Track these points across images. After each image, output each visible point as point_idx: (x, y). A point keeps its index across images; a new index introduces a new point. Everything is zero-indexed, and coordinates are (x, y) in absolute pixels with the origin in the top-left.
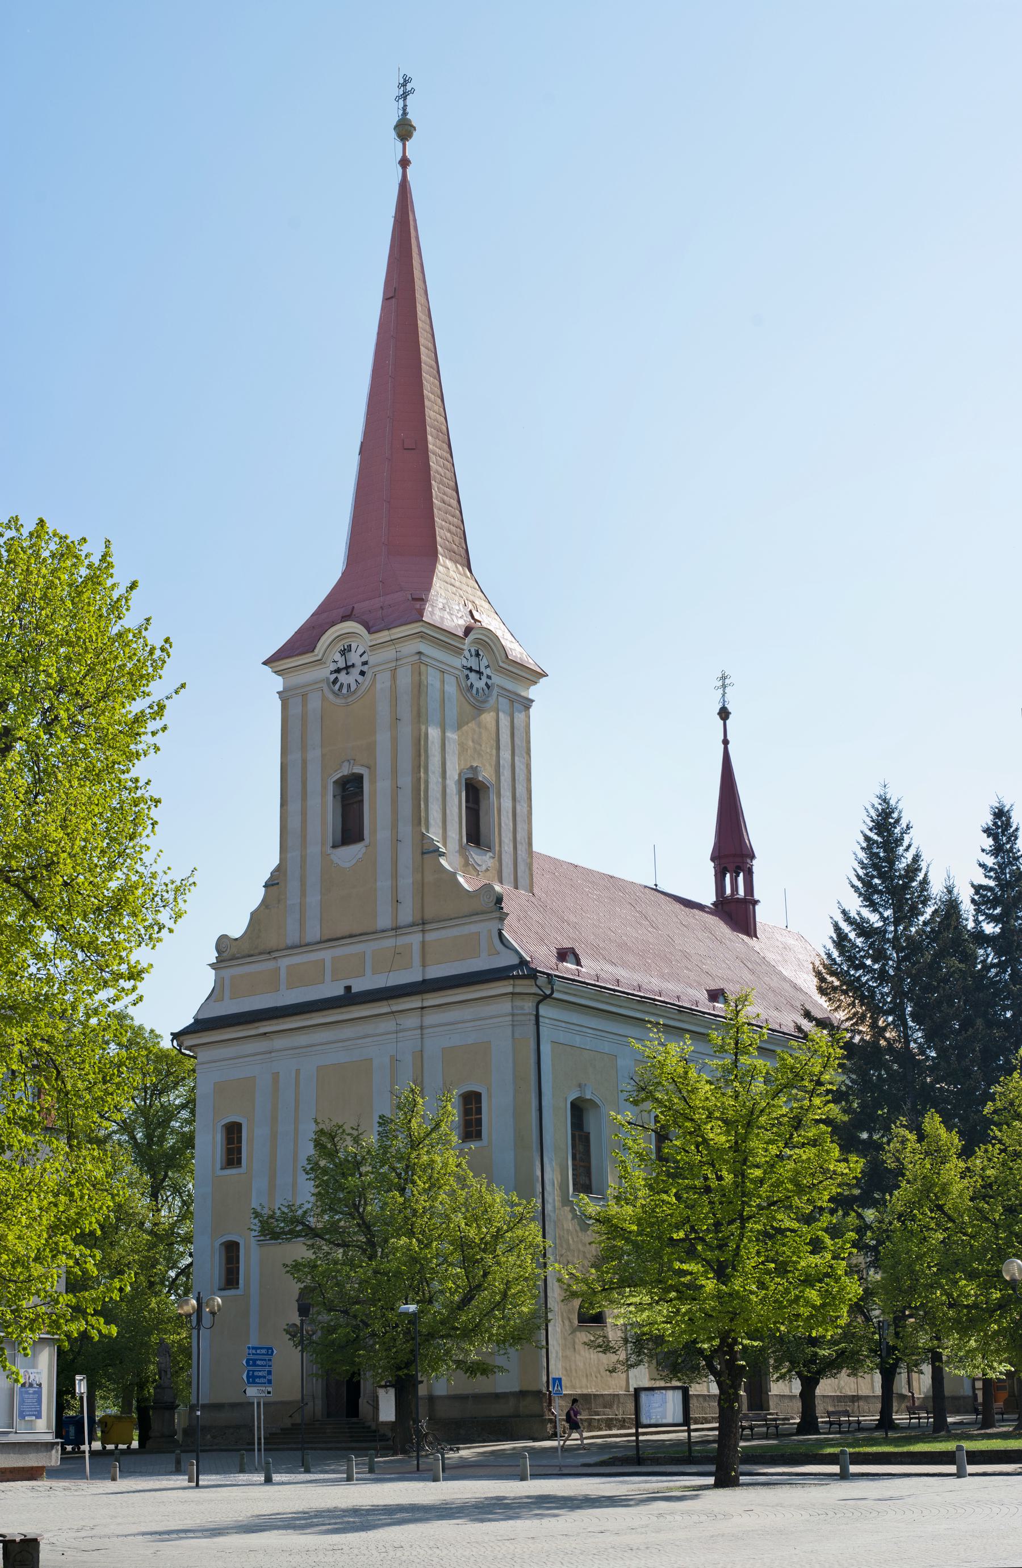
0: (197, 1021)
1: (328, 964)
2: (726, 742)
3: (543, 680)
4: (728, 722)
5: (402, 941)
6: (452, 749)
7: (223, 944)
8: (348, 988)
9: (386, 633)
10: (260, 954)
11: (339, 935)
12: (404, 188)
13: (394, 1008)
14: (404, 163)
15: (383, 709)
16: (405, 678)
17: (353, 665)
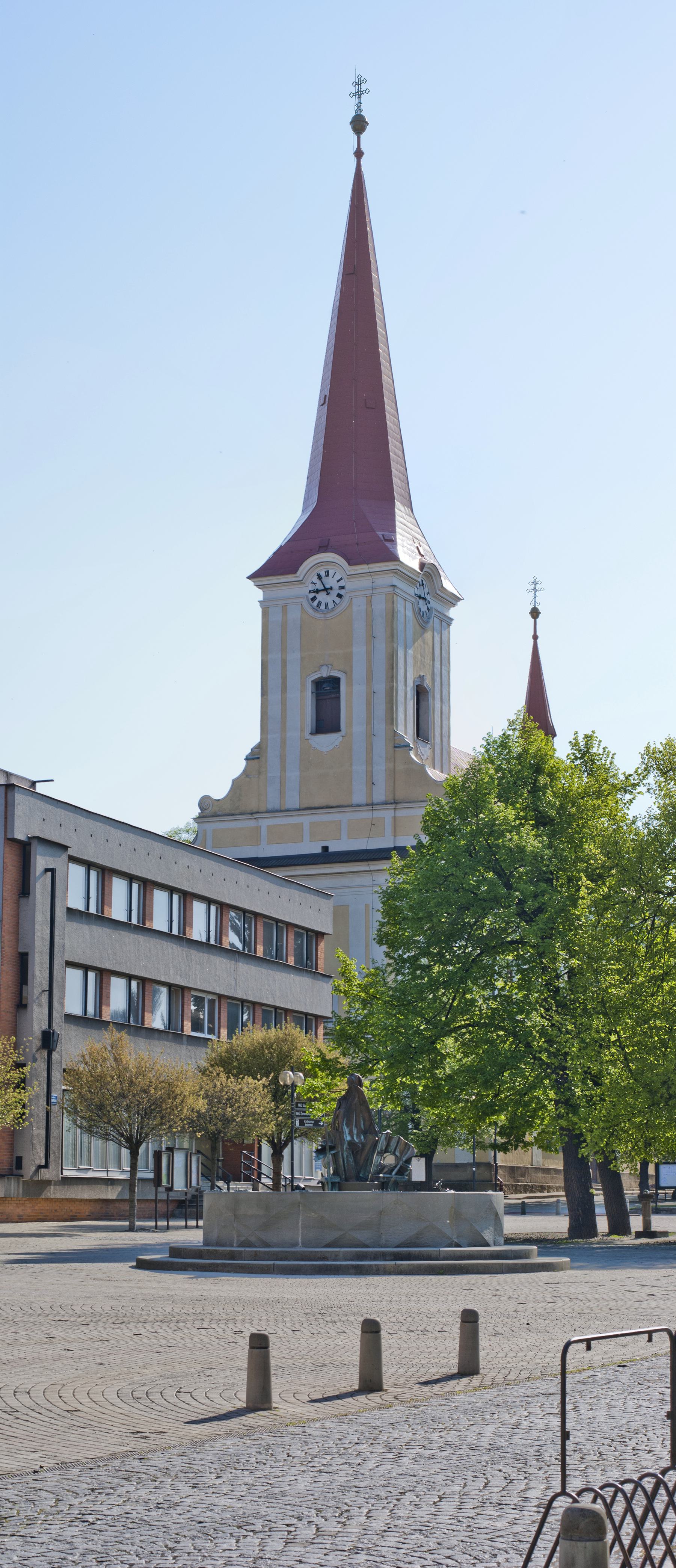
1: (306, 828)
2: (535, 637)
3: (460, 603)
4: (538, 620)
5: (377, 814)
6: (410, 661)
7: (205, 803)
8: (325, 849)
9: (365, 566)
10: (241, 814)
11: (317, 805)
13: (372, 868)
14: (359, 154)
15: (359, 628)
16: (380, 605)
17: (331, 588)
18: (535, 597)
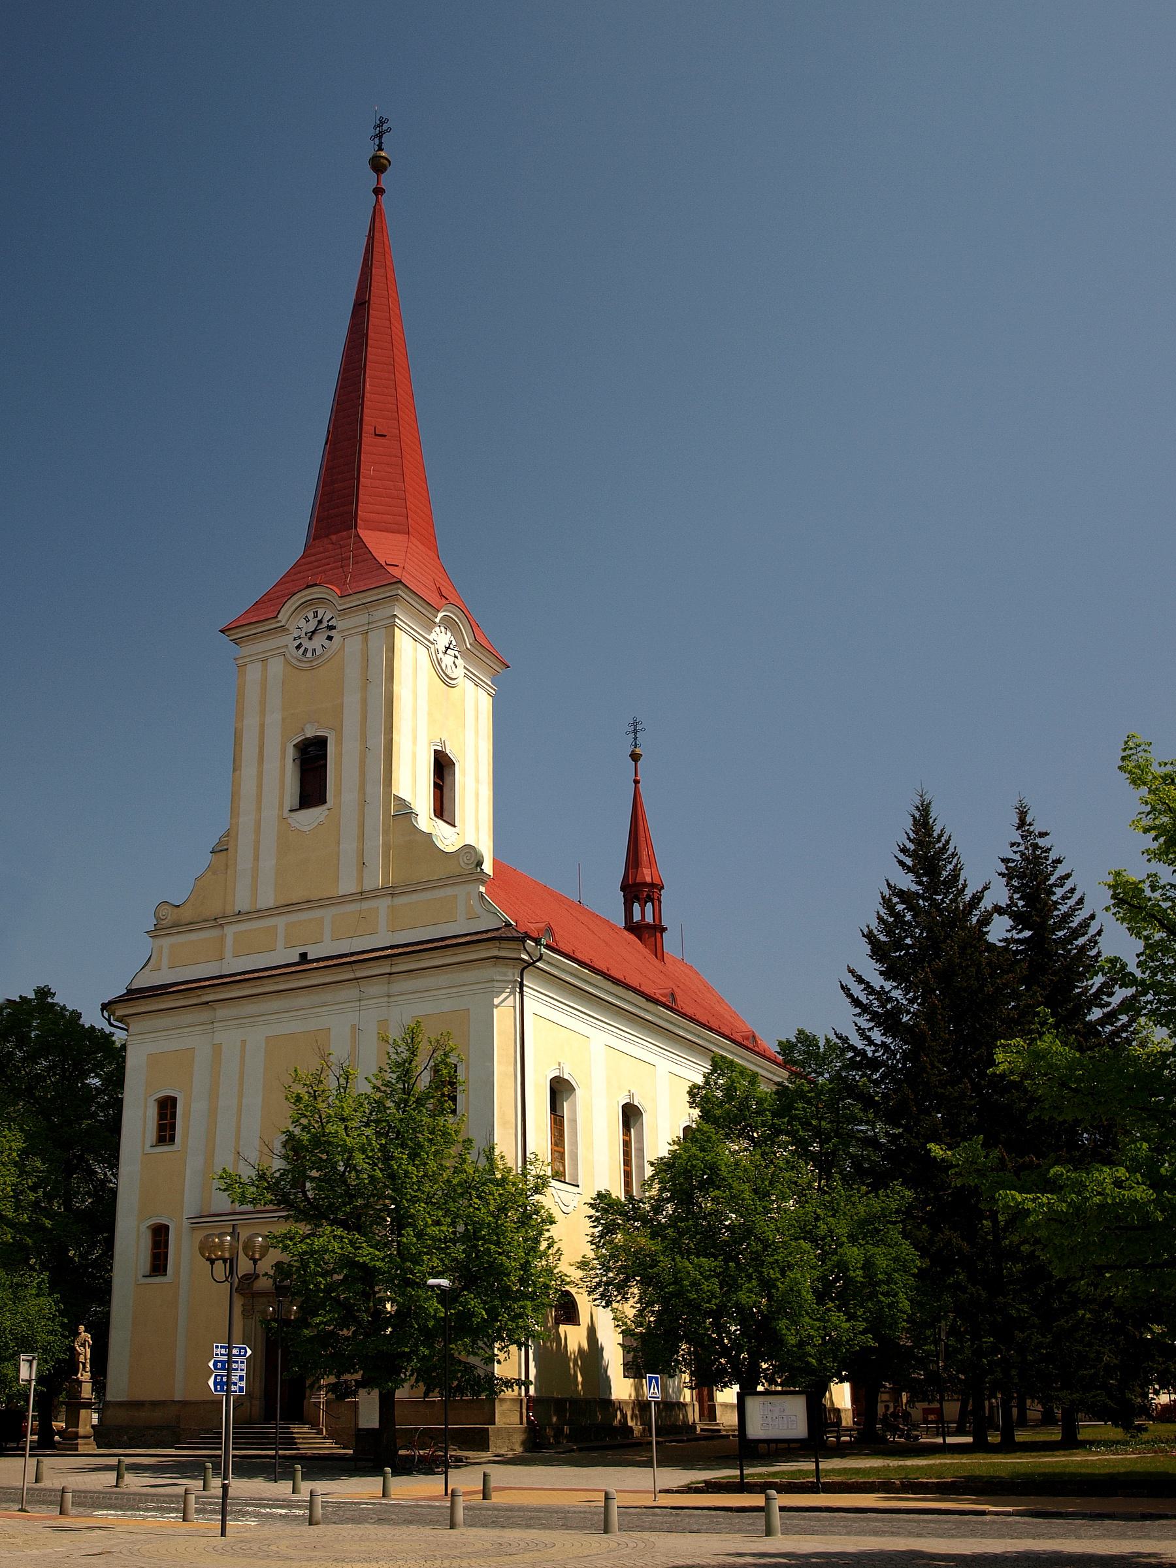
0: (130, 991)
8: (303, 956)
12: (377, 212)
13: (359, 975)
14: (378, 191)
18: (635, 739)
